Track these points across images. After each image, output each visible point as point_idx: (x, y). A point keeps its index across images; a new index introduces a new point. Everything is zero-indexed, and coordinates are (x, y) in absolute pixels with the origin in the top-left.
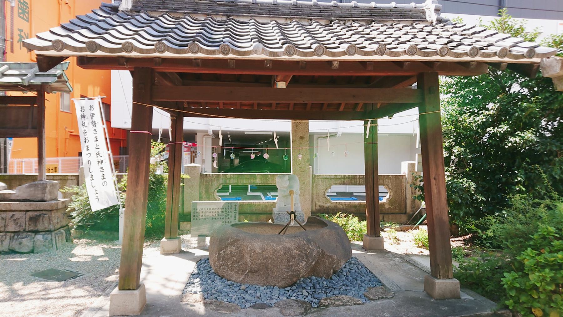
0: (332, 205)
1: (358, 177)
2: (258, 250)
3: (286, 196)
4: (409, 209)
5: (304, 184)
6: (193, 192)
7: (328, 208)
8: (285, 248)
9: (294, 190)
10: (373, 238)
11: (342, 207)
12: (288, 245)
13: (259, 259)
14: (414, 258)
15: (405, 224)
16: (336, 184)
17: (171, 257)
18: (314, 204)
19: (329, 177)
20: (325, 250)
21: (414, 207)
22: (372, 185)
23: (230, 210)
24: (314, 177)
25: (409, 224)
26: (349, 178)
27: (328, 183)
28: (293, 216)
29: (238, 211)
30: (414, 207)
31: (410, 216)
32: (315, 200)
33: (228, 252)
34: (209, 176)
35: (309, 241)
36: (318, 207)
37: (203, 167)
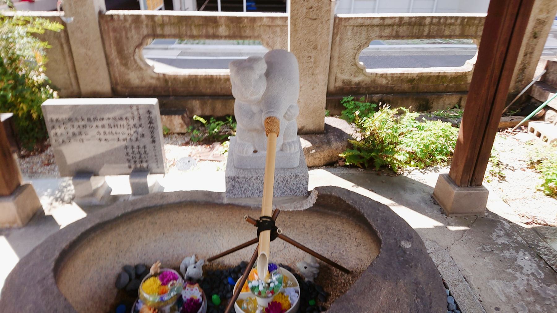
0: (367, 79)
1: (428, 21)
5: (315, 48)
6: (90, 53)
7: (358, 84)
10: (464, 192)
11: (384, 82)
16: (381, 37)
18: (333, 78)
19: (368, 22)
21: (521, 81)
22: (497, 72)
26: (409, 24)
27: (364, 34)
28: (266, 234)
30: (521, 81)
32: (335, 70)
36: (339, 84)
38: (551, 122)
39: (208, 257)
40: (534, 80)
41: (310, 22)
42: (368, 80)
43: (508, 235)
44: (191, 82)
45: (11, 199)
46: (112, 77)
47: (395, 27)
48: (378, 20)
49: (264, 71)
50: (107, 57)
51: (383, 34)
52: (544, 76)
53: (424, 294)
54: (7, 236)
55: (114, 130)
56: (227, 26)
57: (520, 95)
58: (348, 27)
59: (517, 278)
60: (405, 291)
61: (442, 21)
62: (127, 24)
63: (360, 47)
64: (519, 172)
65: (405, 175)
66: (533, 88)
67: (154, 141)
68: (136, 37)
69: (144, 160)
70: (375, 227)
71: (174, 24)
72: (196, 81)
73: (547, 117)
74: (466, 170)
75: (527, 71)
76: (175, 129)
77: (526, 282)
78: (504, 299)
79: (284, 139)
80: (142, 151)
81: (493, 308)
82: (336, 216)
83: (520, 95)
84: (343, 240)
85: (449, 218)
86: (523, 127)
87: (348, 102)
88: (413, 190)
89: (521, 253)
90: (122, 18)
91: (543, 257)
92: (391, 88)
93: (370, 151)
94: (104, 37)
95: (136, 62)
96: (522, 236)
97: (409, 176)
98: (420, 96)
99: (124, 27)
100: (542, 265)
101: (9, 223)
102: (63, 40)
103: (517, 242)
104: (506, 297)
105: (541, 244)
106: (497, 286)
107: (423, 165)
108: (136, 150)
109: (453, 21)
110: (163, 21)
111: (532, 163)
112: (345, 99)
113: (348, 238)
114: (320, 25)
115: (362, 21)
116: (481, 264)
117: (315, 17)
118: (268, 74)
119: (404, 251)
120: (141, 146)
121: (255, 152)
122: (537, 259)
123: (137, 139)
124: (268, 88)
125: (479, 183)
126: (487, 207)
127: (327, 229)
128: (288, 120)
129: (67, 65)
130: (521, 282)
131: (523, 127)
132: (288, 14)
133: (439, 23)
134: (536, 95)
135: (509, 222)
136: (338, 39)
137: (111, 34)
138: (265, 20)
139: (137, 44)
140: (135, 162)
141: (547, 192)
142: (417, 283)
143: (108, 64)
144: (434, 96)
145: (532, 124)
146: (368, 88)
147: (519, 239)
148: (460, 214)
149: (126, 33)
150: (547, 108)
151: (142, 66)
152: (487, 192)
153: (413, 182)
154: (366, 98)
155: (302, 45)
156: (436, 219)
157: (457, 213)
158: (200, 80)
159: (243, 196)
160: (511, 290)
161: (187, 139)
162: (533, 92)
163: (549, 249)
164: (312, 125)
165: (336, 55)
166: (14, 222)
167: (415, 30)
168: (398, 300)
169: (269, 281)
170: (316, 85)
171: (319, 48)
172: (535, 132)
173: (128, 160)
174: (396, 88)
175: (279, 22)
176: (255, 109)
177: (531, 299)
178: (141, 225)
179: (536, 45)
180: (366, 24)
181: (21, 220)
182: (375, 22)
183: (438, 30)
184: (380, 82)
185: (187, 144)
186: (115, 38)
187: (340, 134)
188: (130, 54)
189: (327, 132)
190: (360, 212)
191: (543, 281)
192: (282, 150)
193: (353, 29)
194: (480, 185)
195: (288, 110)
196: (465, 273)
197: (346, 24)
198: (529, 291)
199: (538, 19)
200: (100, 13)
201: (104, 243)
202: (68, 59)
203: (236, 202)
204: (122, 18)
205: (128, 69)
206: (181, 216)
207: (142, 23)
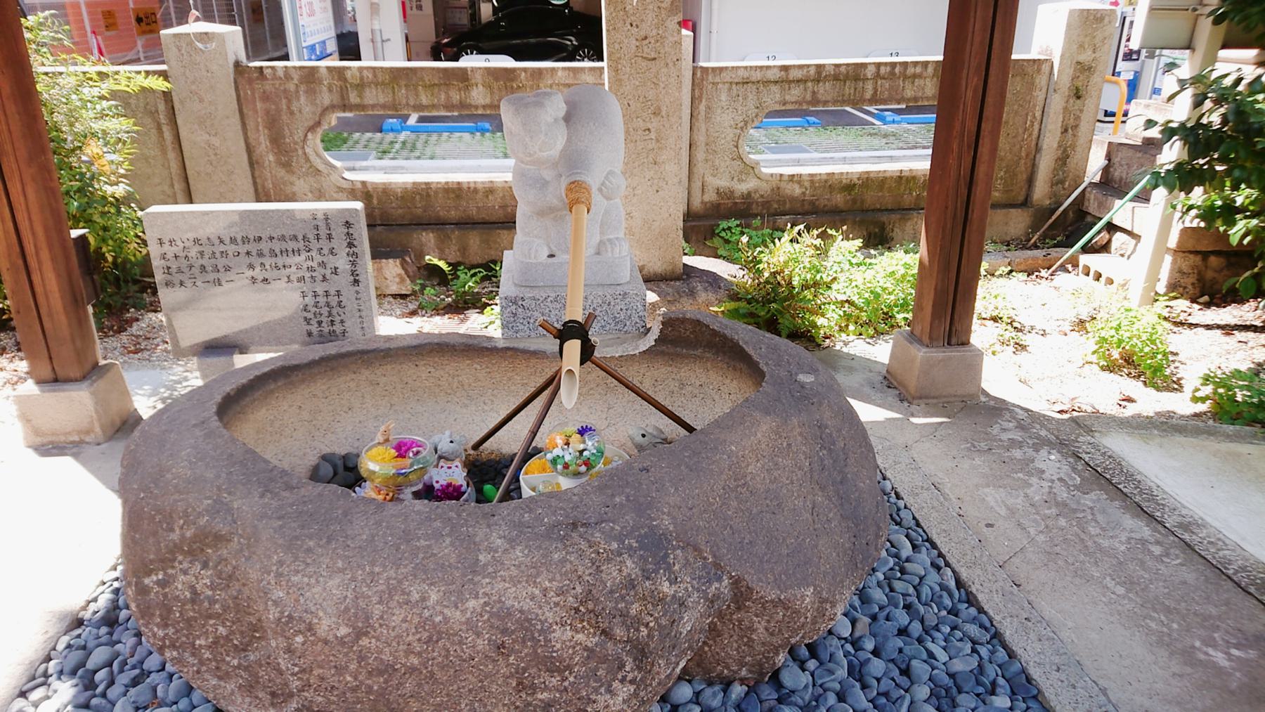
1: (870, 72)
2: (326, 624)
3: (552, 210)
4: (1041, 191)
5: (657, 113)
6: (216, 141)
8: (500, 615)
9: (593, 179)
10: (938, 354)
11: (797, 191)
12: (519, 597)
13: (340, 670)
14: (1121, 445)
15: (1025, 248)
17: (66, 464)
18: (697, 185)
19: (757, 76)
20: (751, 579)
21: (1062, 182)
22: (971, 125)
23: (324, 243)
24: (701, 77)
25: (1036, 247)
26: (836, 78)
28: (573, 347)
29: (365, 246)
30: (1062, 182)
31: (1043, 214)
32: (700, 168)
33: (180, 586)
34: (275, 77)
35: (654, 549)
36: (711, 196)
37: (377, 27)
38: (1122, 255)
39: (472, 443)
40: (1087, 181)
41: (644, 64)
42: (765, 188)
43: (1021, 427)
44: (418, 197)
45: (86, 384)
46: (260, 190)
47: (810, 84)
48: (776, 70)
49: (562, 113)
50: (249, 150)
51: (787, 98)
52: (1106, 170)
53: (834, 444)
54: (76, 456)
55: (280, 261)
56: (488, 87)
57: (1061, 209)
58: (720, 86)
59: (1031, 485)
60: (800, 434)
61: (897, 70)
62: (292, 87)
63: (746, 123)
64: (1054, 339)
65: (838, 348)
66: (1087, 195)
67: (356, 282)
68: (307, 109)
69: (337, 319)
70: (755, 357)
71: (383, 83)
72: (428, 195)
73: (1114, 245)
74: (937, 314)
75: (1072, 163)
76: (387, 287)
77: (1047, 490)
78: (1003, 512)
79: (602, 233)
80: (334, 301)
81: (982, 525)
82: (696, 357)
83: (1061, 209)
84: (708, 402)
85: (913, 407)
86: (1069, 267)
87: (729, 228)
88: (851, 370)
89: (1044, 453)
90: (281, 73)
91: (1083, 456)
92: (812, 203)
93: (767, 301)
94: (245, 111)
95: (307, 160)
96: (1048, 430)
97: (845, 350)
98: (866, 213)
99: (285, 91)
100: (1080, 468)
101: (79, 432)
102: (163, 119)
103: (1038, 437)
104: (1008, 509)
105: (1081, 439)
106: (993, 496)
107: (871, 331)
108: (322, 300)
109: (918, 70)
110: (362, 78)
111: (1082, 322)
112: (724, 224)
113: (717, 397)
114: (664, 70)
115: (746, 74)
116: (966, 466)
117: (653, 55)
118: (568, 119)
119: (802, 386)
120: (333, 292)
121: (552, 256)
122: (1071, 460)
123: (324, 279)
124: (569, 140)
125: (964, 339)
126: (984, 385)
127: (682, 385)
128: (608, 198)
129: (169, 168)
130: (1038, 490)
131: (1069, 267)
132: (604, 64)
133: (892, 73)
134: (1092, 207)
135: (1027, 410)
136: (702, 107)
137: (259, 105)
138: (560, 73)
139: (311, 123)
140: (320, 323)
141: (1103, 363)
142: (821, 427)
143: (252, 164)
144: (894, 217)
145: (1085, 259)
146: (766, 204)
147: (1043, 433)
148: (934, 398)
149: (289, 101)
150: (1112, 228)
151: (321, 167)
152: (979, 355)
153: (853, 358)
154: (763, 223)
155: (633, 107)
156: (890, 408)
157: (927, 397)
158: (436, 192)
159: (533, 334)
160: (1018, 501)
161: (412, 307)
162: (1086, 204)
163: (1095, 446)
164: (659, 264)
165: (701, 138)
166: (88, 432)
167: (848, 89)
168: (789, 445)
169: (582, 447)
170: (662, 184)
171: (664, 113)
172: (1092, 273)
173: (305, 319)
174: (822, 202)
175: (589, 79)
176: (548, 174)
177: (1054, 511)
178: (352, 385)
179: (1081, 111)
180: (754, 79)
181: (102, 427)
182: (771, 75)
183: (891, 87)
184: (788, 192)
185: (413, 313)
186: (267, 112)
187: (713, 280)
188: (296, 143)
189: (689, 276)
190: (732, 340)
191: (1077, 487)
192: (598, 253)
193: (730, 89)
194: (966, 343)
195: (607, 178)
196: (936, 480)
197: (717, 80)
198: (1051, 499)
199: (1078, 63)
200: (237, 64)
201: (290, 406)
202: (172, 155)
203: (521, 345)
204: (281, 73)
205: (291, 172)
206: (421, 373)
207: (321, 82)
